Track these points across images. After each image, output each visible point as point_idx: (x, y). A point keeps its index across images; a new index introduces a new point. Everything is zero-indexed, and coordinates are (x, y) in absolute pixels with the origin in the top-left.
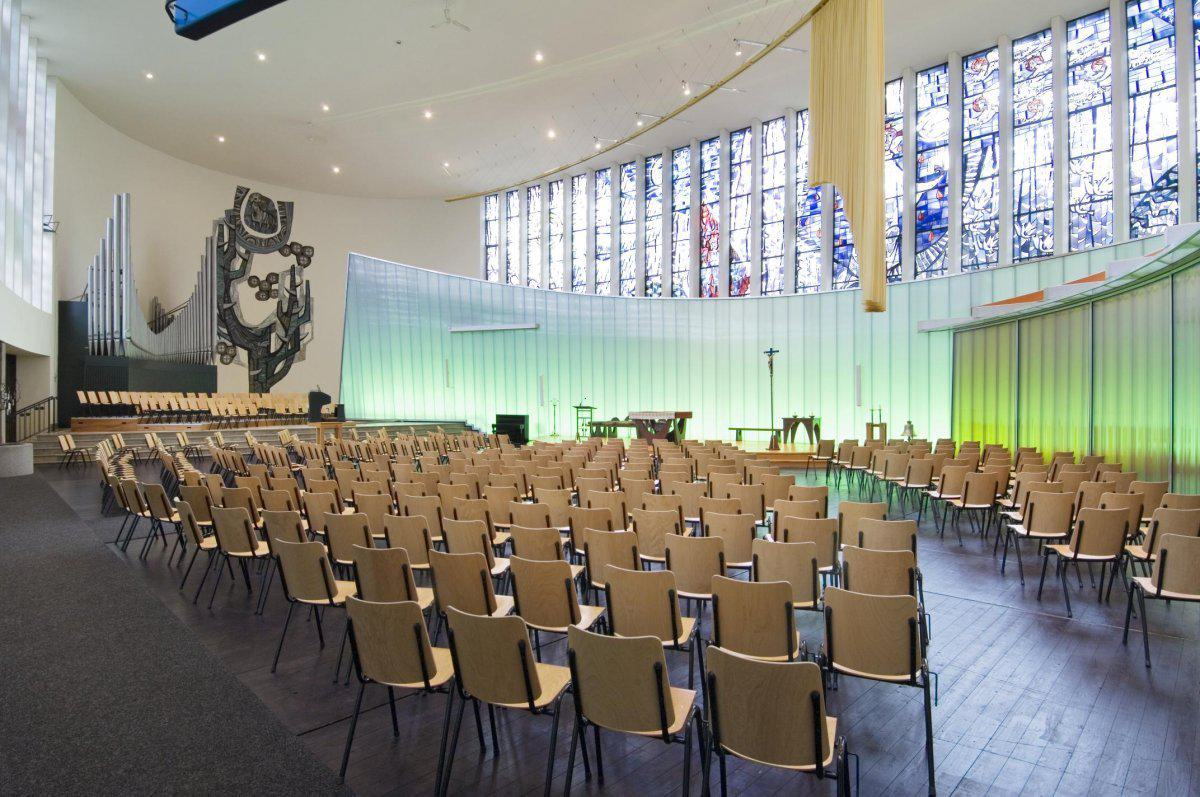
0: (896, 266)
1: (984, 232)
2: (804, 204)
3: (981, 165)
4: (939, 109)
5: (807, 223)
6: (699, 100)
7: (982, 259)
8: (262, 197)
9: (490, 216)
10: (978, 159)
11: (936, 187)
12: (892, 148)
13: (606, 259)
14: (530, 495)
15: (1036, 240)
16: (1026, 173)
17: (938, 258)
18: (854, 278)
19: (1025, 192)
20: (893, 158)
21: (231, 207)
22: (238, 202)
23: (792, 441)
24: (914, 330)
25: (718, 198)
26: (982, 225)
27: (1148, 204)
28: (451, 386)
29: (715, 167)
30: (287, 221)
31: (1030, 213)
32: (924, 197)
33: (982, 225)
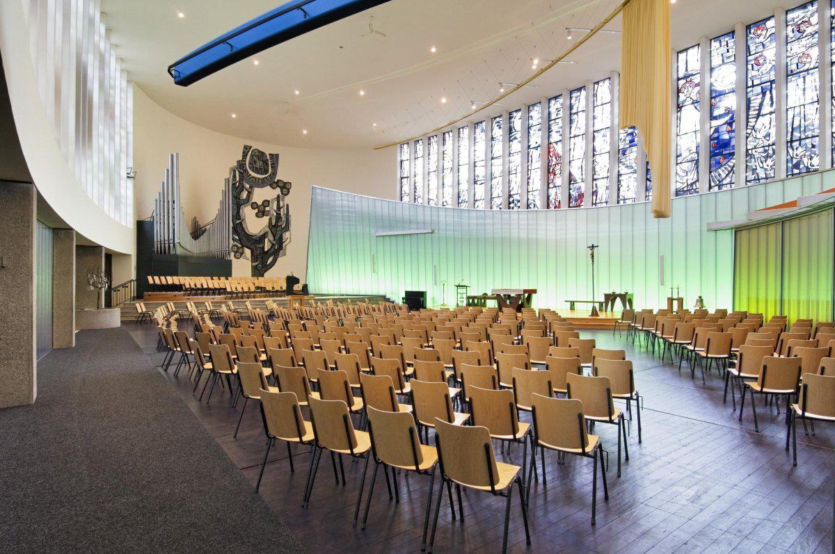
0: (695, 182)
5: (627, 152)
8: (259, 152)
9: (404, 158)
15: (805, 160)
16: (797, 110)
17: (727, 175)
21: (240, 158)
22: (245, 155)
23: (612, 310)
24: (705, 228)
26: (762, 149)
30: (275, 167)
31: (800, 139)
33: (762, 149)
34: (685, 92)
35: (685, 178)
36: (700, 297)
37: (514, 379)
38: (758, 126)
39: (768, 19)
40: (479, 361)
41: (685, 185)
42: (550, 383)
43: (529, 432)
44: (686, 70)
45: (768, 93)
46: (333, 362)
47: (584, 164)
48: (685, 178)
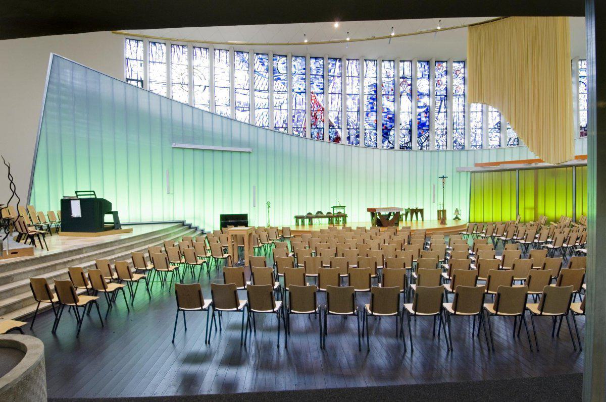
0: (409, 142)
1: (442, 133)
2: (368, 106)
3: (440, 106)
4: (424, 79)
5: (370, 115)
6: (376, 39)
7: (441, 144)
10: (439, 104)
11: (424, 112)
12: (406, 90)
13: (244, 111)
14: (115, 276)
15: (459, 140)
16: (456, 114)
17: (425, 141)
18: (391, 145)
19: (455, 121)
20: (407, 95)
24: (455, 170)
25: (322, 91)
26: (441, 131)
27: (492, 133)
28: (171, 192)
29: (319, 74)
31: (457, 129)
32: (419, 115)
33: (441, 131)
34: (403, 86)
35: (403, 139)
36: (457, 209)
37: (305, 262)
38: (439, 117)
39: (444, 62)
40: (343, 254)
41: (403, 143)
42: (348, 263)
43: (246, 305)
44: (404, 74)
45: (443, 101)
46: (304, 262)
47: (340, 115)
48: (403, 139)
